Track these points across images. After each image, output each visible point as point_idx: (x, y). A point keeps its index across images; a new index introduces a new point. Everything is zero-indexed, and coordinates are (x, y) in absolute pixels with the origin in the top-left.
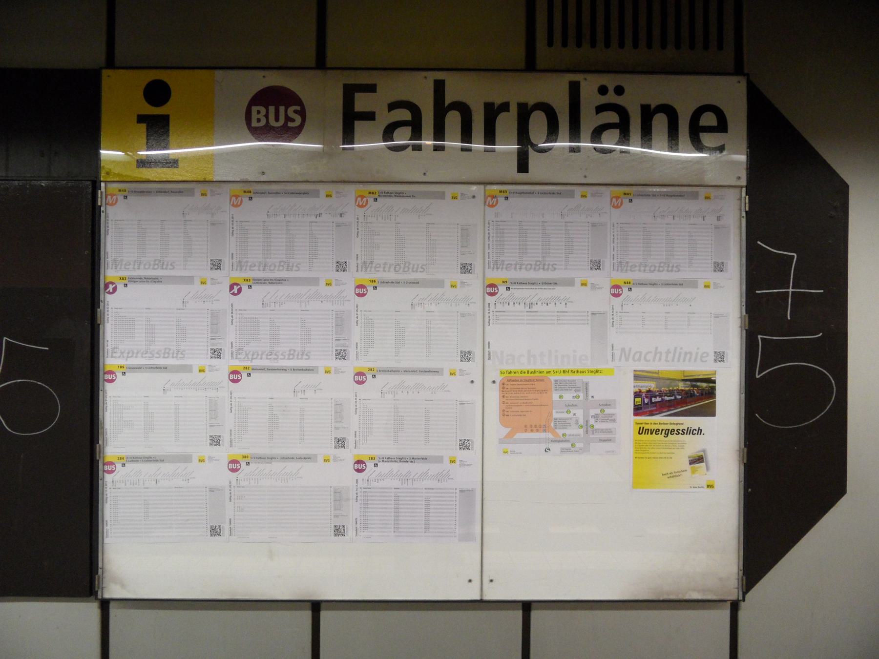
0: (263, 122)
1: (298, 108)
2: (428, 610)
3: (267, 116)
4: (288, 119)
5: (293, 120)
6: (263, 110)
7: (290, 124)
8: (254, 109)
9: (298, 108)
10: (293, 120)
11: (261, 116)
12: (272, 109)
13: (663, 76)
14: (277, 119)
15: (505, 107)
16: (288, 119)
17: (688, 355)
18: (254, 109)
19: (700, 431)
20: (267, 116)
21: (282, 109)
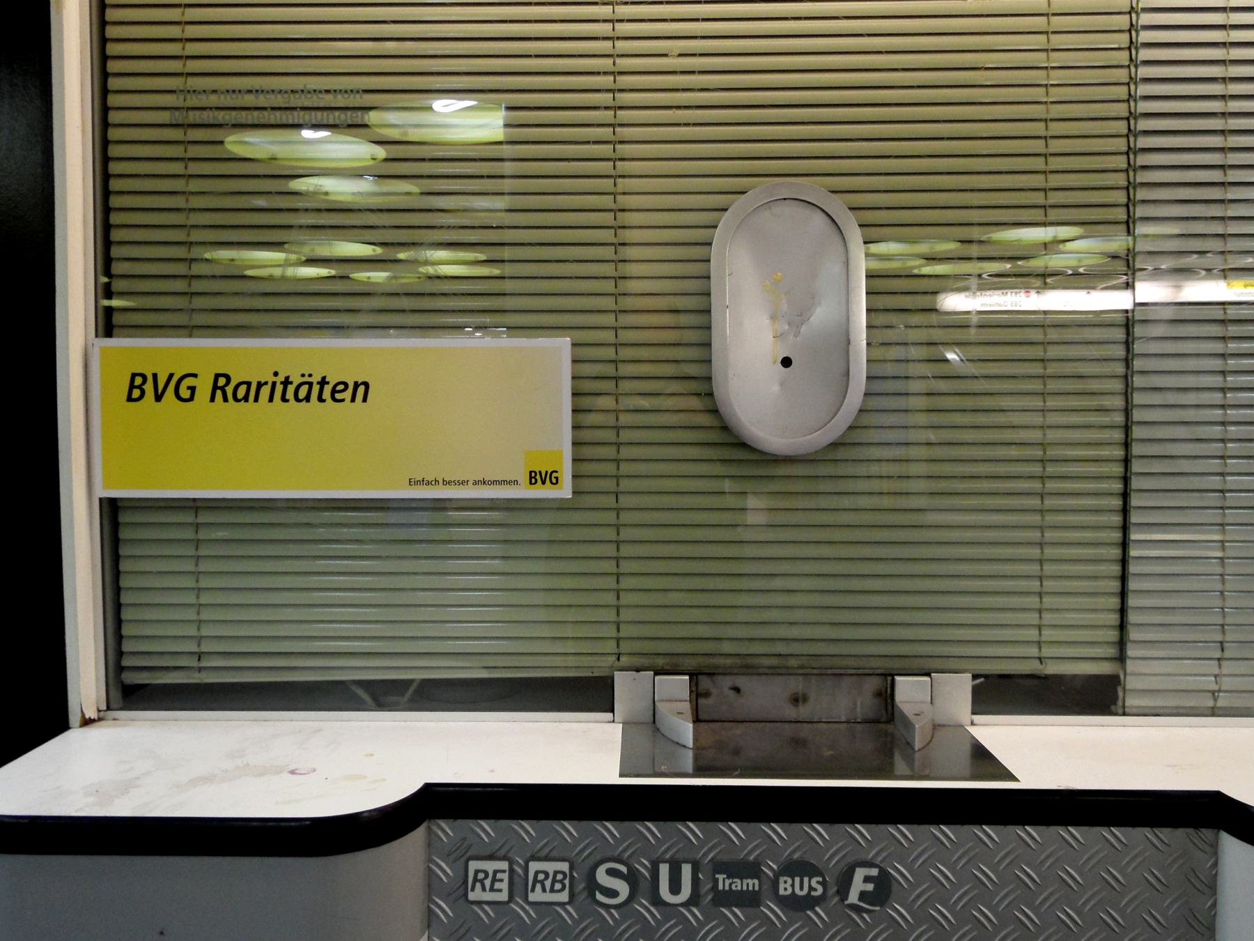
0: (790, 891)
1: (820, 879)
2: (64, 116)
3: (793, 886)
4: (811, 888)
5: (815, 890)
6: (790, 881)
7: (813, 893)
8: (782, 879)
9: (820, 879)
10: (815, 890)
11: (788, 886)
12: (797, 880)
13: (91, 595)
14: (801, 889)
15: (266, 383)
16: (811, 888)
17: (361, 389)
18: (782, 879)
19: (361, 389)
20: (793, 886)
21: (806, 879)
